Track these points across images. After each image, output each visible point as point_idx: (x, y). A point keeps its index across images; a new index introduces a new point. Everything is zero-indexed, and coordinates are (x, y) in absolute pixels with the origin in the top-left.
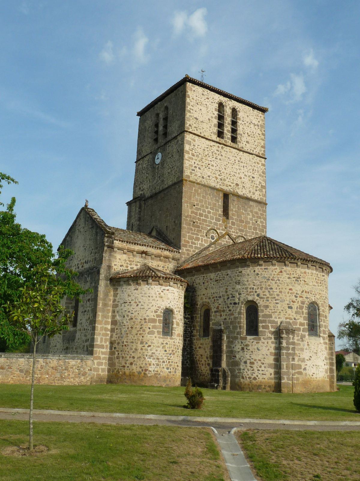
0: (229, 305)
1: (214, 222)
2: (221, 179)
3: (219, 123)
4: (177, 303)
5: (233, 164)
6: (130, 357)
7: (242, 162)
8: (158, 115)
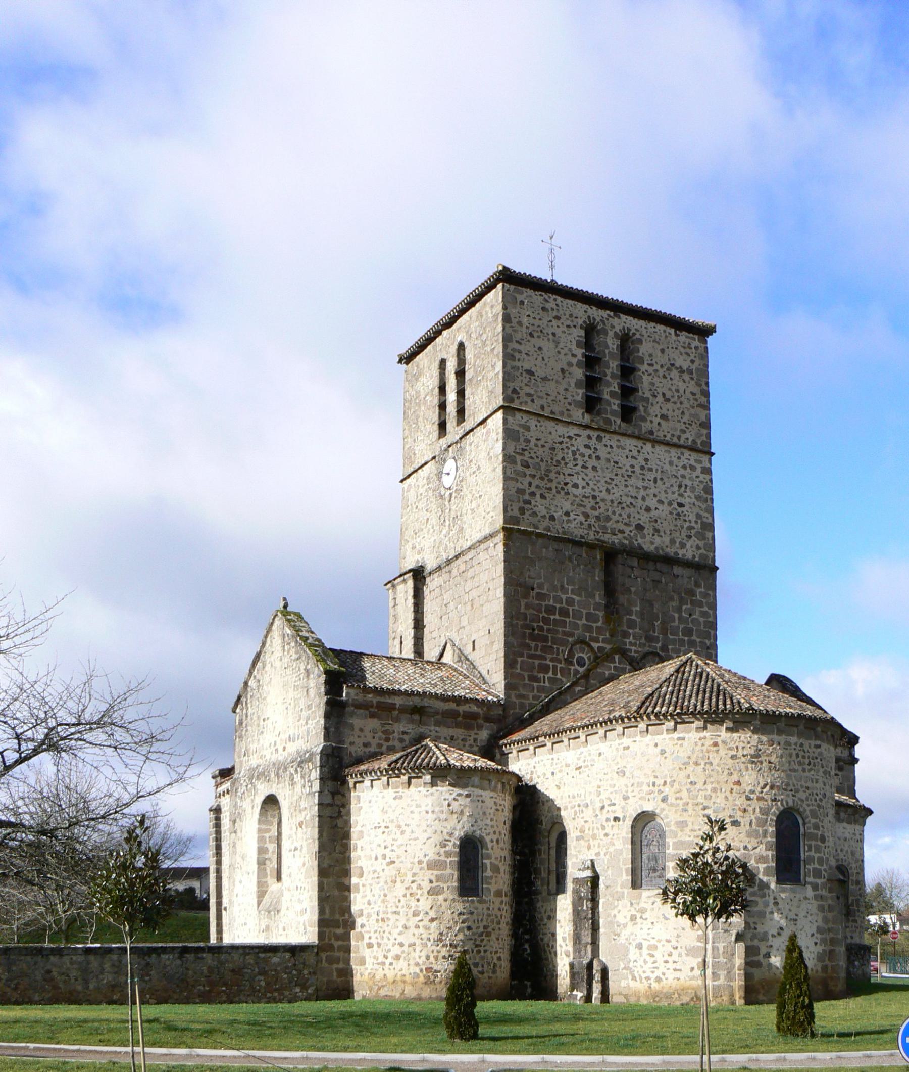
0: (604, 823)
1: (584, 625)
2: (598, 518)
3: (587, 376)
4: (492, 823)
5: (628, 476)
6: (394, 945)
7: (651, 470)
8: (443, 362)
